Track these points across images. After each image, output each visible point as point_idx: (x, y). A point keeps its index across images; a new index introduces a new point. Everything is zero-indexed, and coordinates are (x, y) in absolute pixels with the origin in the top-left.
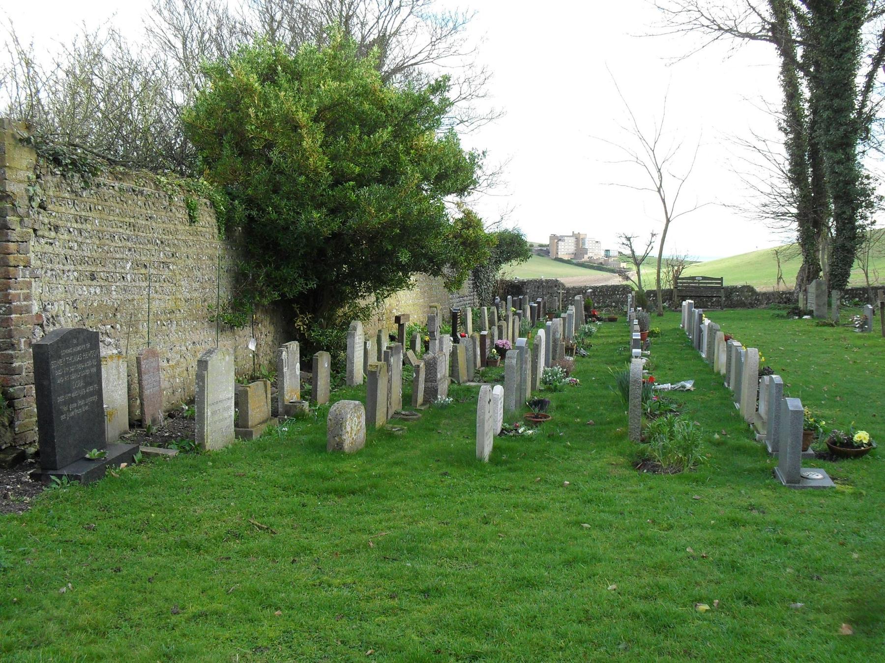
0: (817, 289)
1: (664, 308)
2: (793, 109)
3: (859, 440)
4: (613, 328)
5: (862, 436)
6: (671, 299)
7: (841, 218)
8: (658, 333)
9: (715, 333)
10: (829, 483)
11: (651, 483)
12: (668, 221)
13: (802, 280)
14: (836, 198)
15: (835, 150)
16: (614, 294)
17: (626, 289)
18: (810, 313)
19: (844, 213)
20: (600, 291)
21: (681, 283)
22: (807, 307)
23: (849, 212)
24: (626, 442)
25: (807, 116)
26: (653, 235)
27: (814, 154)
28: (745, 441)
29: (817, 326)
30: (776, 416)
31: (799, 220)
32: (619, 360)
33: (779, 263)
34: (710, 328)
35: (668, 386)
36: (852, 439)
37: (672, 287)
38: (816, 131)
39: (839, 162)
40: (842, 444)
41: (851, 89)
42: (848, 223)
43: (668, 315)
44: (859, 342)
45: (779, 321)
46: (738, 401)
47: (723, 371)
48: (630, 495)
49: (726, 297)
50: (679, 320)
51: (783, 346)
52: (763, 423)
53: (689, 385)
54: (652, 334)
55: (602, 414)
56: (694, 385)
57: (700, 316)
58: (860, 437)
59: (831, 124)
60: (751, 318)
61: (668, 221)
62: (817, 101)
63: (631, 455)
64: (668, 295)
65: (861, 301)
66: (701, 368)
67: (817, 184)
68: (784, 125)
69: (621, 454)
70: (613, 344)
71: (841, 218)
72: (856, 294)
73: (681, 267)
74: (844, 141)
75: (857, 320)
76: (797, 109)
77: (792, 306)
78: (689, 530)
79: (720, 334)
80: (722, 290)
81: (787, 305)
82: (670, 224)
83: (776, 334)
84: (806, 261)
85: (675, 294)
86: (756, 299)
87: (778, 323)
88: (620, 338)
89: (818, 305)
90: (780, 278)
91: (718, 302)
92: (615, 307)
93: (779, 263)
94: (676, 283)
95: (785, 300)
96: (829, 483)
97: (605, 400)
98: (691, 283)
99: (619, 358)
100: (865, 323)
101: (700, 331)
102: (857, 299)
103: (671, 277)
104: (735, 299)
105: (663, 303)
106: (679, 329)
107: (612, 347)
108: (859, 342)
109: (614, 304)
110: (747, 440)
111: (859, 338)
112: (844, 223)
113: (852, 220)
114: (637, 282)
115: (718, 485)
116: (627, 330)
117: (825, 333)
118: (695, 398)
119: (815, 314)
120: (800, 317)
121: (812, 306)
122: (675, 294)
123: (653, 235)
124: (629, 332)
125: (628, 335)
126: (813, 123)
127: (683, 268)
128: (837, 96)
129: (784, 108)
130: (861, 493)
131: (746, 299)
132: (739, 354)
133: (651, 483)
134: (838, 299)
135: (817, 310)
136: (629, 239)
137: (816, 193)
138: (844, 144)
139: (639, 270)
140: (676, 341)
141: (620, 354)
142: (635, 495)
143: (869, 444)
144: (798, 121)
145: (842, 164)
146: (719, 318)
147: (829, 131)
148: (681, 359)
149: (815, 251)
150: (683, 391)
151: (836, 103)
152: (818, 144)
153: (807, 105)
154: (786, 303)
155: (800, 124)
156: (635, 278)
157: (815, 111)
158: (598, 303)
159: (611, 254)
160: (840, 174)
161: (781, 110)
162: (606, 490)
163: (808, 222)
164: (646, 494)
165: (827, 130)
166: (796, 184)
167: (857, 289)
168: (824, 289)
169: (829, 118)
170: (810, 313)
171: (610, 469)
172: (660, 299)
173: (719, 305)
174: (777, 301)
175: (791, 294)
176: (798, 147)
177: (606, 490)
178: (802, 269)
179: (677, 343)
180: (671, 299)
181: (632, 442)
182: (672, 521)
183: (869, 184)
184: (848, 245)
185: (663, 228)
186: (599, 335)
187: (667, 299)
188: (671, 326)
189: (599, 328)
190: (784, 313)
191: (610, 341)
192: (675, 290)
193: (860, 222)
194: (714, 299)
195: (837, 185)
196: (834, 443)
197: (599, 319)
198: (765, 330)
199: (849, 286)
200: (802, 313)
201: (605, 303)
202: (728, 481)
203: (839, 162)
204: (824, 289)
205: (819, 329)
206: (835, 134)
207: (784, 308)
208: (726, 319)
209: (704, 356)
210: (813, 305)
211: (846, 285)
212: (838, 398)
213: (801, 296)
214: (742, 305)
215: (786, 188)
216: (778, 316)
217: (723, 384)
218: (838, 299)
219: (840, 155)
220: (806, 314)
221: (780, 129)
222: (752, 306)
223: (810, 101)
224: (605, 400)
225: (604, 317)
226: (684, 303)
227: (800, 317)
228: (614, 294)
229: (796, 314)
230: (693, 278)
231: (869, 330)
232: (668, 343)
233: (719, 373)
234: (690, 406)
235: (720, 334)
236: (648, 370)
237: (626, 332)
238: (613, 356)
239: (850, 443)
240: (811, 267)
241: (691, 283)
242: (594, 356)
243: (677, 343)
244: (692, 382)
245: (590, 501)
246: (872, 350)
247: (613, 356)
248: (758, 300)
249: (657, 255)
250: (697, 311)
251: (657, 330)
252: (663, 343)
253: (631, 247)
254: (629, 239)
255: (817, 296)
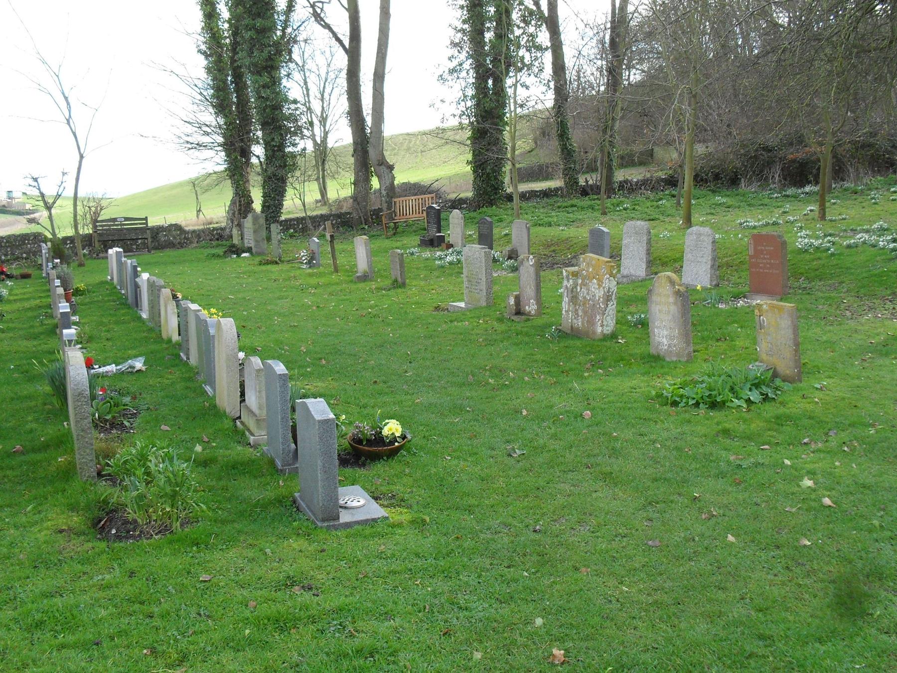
0: (254, 224)
1: (84, 255)
2: (211, 29)
3: (390, 433)
4: (28, 287)
5: (392, 428)
6: (90, 245)
7: (270, 145)
8: (84, 291)
9: (159, 290)
10: (376, 511)
11: (132, 563)
12: (82, 157)
13: (234, 214)
14: (264, 125)
15: (259, 73)
16: (25, 244)
17: (38, 238)
18: (249, 250)
19: (273, 139)
20: (7, 242)
21: (101, 226)
22: (243, 243)
23: (277, 139)
24: (76, 485)
25: (226, 37)
26: (64, 174)
27: (238, 77)
28: (238, 451)
29: (260, 264)
30: (282, 419)
31: (226, 150)
32: (42, 333)
33: (197, 195)
34: (151, 285)
35: (112, 368)
36: (381, 432)
37: (91, 232)
38: (238, 53)
39: (265, 86)
40: (369, 441)
41: (273, 8)
42: (277, 151)
43: (90, 264)
44: (313, 281)
45: (216, 261)
46: (212, 382)
47: (175, 338)
48: (101, 594)
49: (152, 237)
50: (106, 270)
51: (231, 293)
52: (258, 421)
53: (139, 364)
54: (77, 292)
55: (31, 431)
56: (145, 364)
57: (135, 268)
58: (391, 429)
59: (254, 46)
60: (184, 261)
61: (82, 157)
62: (238, 21)
63: (88, 508)
64: (88, 240)
65: (296, 232)
66: (145, 334)
67: (242, 110)
68: (203, 47)
69: (73, 508)
70: (31, 309)
71: (270, 145)
72: (290, 225)
73: (99, 209)
74: (269, 63)
75: (304, 256)
76: (216, 29)
77: (228, 243)
78: (215, 658)
79: (166, 292)
80: (148, 231)
81: (220, 242)
82: (84, 161)
83: (219, 278)
84: (236, 194)
85: (96, 239)
86: (185, 238)
87: (216, 264)
88: (38, 301)
89: (256, 241)
90: (199, 211)
91: (144, 244)
92: (26, 259)
93: (197, 195)
94: (95, 227)
95: (216, 237)
96: (376, 511)
97: (33, 403)
98: (113, 225)
99: (41, 329)
100: (312, 258)
101: (137, 286)
102: (292, 231)
103: (89, 220)
104: (163, 239)
105: (83, 250)
106: (106, 282)
107: (30, 314)
108: (313, 281)
109: (24, 255)
110: (239, 448)
111: (311, 275)
112: (274, 151)
113: (281, 146)
114: (50, 228)
115: (231, 542)
116: (44, 288)
117: (272, 272)
118: (151, 383)
119: (254, 250)
120: (239, 255)
121: (249, 241)
122: (96, 239)
123: (64, 174)
124: (49, 291)
125: (48, 296)
126: (235, 46)
127: (101, 209)
128: (259, 15)
129: (203, 28)
130: (424, 521)
131: (174, 238)
132: (202, 325)
133: (132, 563)
134: (278, 234)
135: (256, 246)
136: (36, 180)
137: (242, 120)
138: (269, 67)
139: (51, 214)
140: (106, 299)
141: (42, 324)
142: (110, 593)
143: (403, 437)
144: (218, 42)
145: (268, 88)
146: (149, 264)
147: (253, 53)
148: (117, 323)
149: (245, 183)
150: (132, 372)
151: (259, 23)
152: (240, 67)
153: (226, 26)
154: (218, 239)
155: (220, 46)
156: (46, 222)
157: (235, 33)
158: (6, 255)
159: (14, 195)
160: (267, 99)
161: (199, 30)
162: (59, 592)
163: (235, 150)
164: (127, 589)
165: (251, 53)
166: (220, 111)
167: (291, 220)
168: (261, 223)
169: (252, 39)
170: (249, 250)
171: (61, 540)
172: (79, 245)
173: (146, 247)
174: (208, 238)
175: (222, 229)
176: (219, 71)
177: (59, 592)
178: (233, 202)
179: (109, 301)
180: (90, 245)
181: (85, 483)
182: (183, 644)
183: (296, 109)
184: (281, 173)
185: (77, 166)
186: (11, 298)
187: (86, 245)
188: (97, 278)
189: (11, 290)
190: (220, 251)
191: (27, 305)
192: (95, 234)
193: (290, 149)
194: (140, 241)
195: (264, 110)
196: (360, 441)
197: (10, 277)
198: (205, 274)
199: (283, 218)
200: (239, 251)
201: (13, 254)
202: (239, 532)
203: (265, 86)
204: (261, 223)
205: (264, 268)
206: (259, 56)
207: (218, 246)
208: (156, 264)
209: (145, 316)
210: (251, 241)
211: (280, 216)
212: (324, 362)
213: (235, 232)
214: (171, 245)
215: (209, 117)
216: (214, 255)
217: (180, 356)
218: (278, 234)
219: (266, 79)
220: (244, 252)
221: (200, 51)
222: (181, 245)
223: (229, 21)
224: (33, 403)
225: (15, 273)
226: (110, 251)
227: (239, 255)
228: (25, 244)
229: (234, 253)
230: (114, 220)
231: (318, 265)
232: (98, 301)
233: (170, 341)
234: (148, 397)
235: (166, 292)
236: (81, 343)
237: (44, 291)
238: (32, 327)
239: (379, 440)
240: (242, 199)
241: (113, 225)
242: (9, 329)
243: (109, 301)
244: (142, 359)
245: (39, 625)
246: (329, 290)
247: (32, 327)
248: (187, 239)
249: (72, 195)
250: (129, 261)
251: (81, 286)
252: (91, 303)
253: (39, 189)
254: (36, 180)
255: (254, 232)
